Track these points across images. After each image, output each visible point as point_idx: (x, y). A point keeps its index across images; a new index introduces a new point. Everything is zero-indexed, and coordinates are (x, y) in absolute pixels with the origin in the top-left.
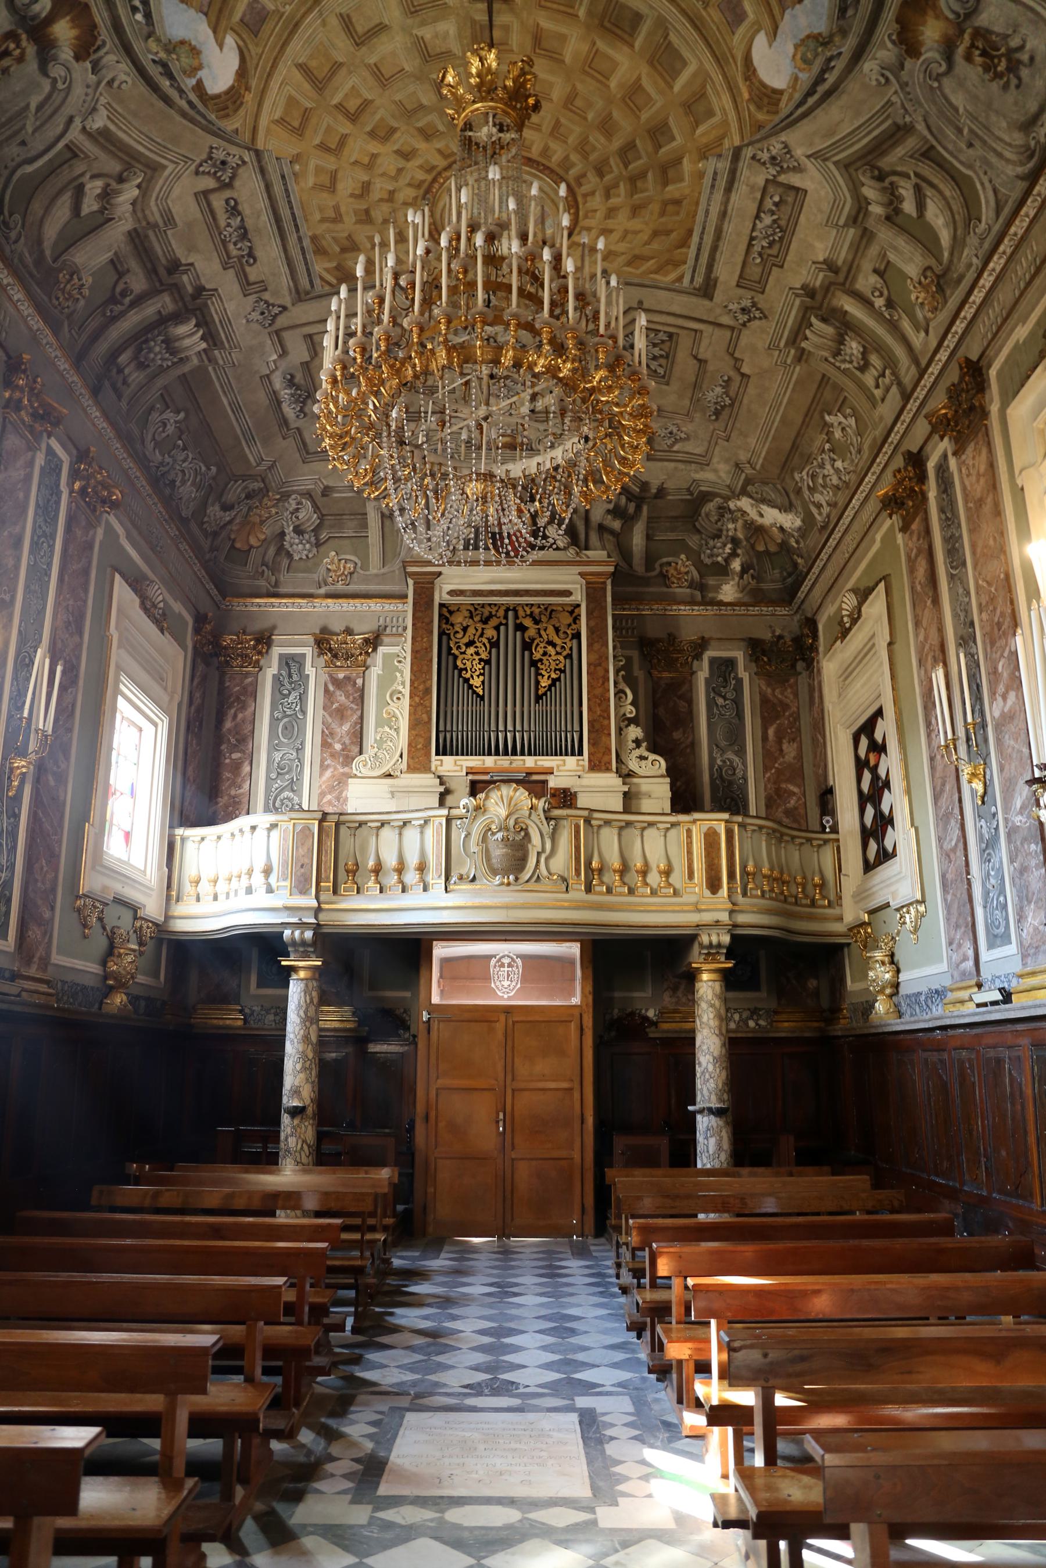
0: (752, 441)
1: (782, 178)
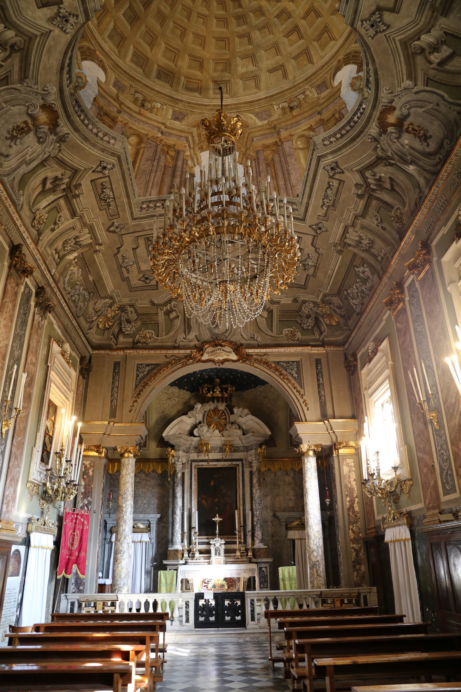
1: (55, 8)
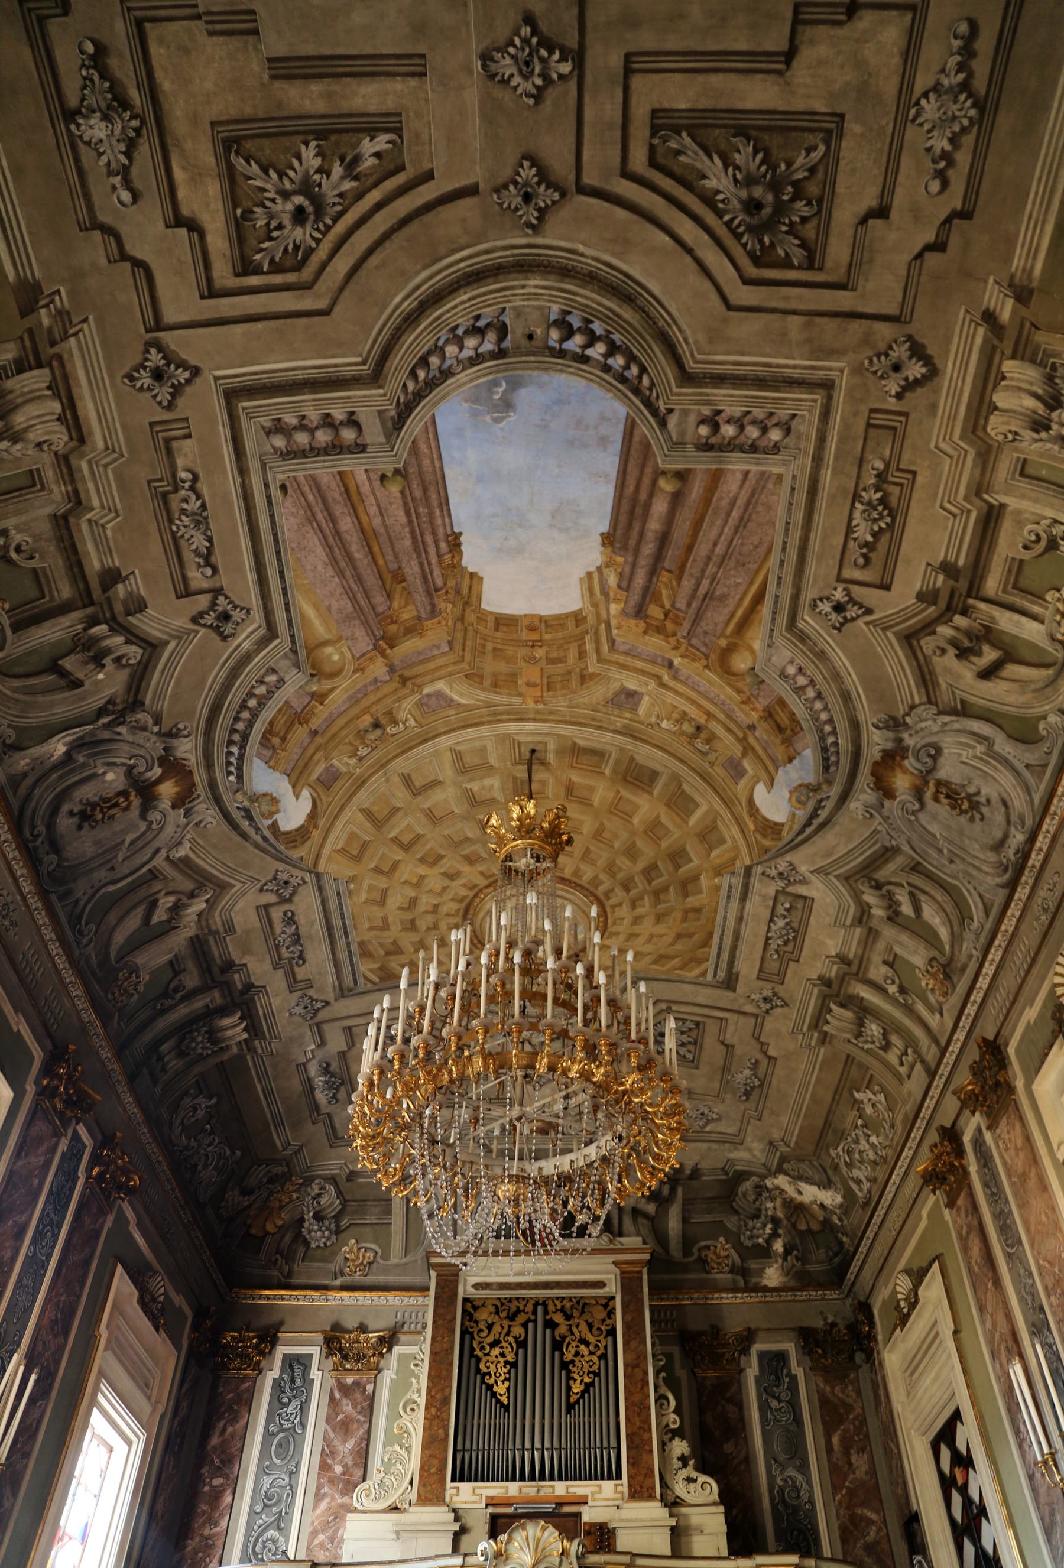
0: (784, 1120)
1: (790, 889)
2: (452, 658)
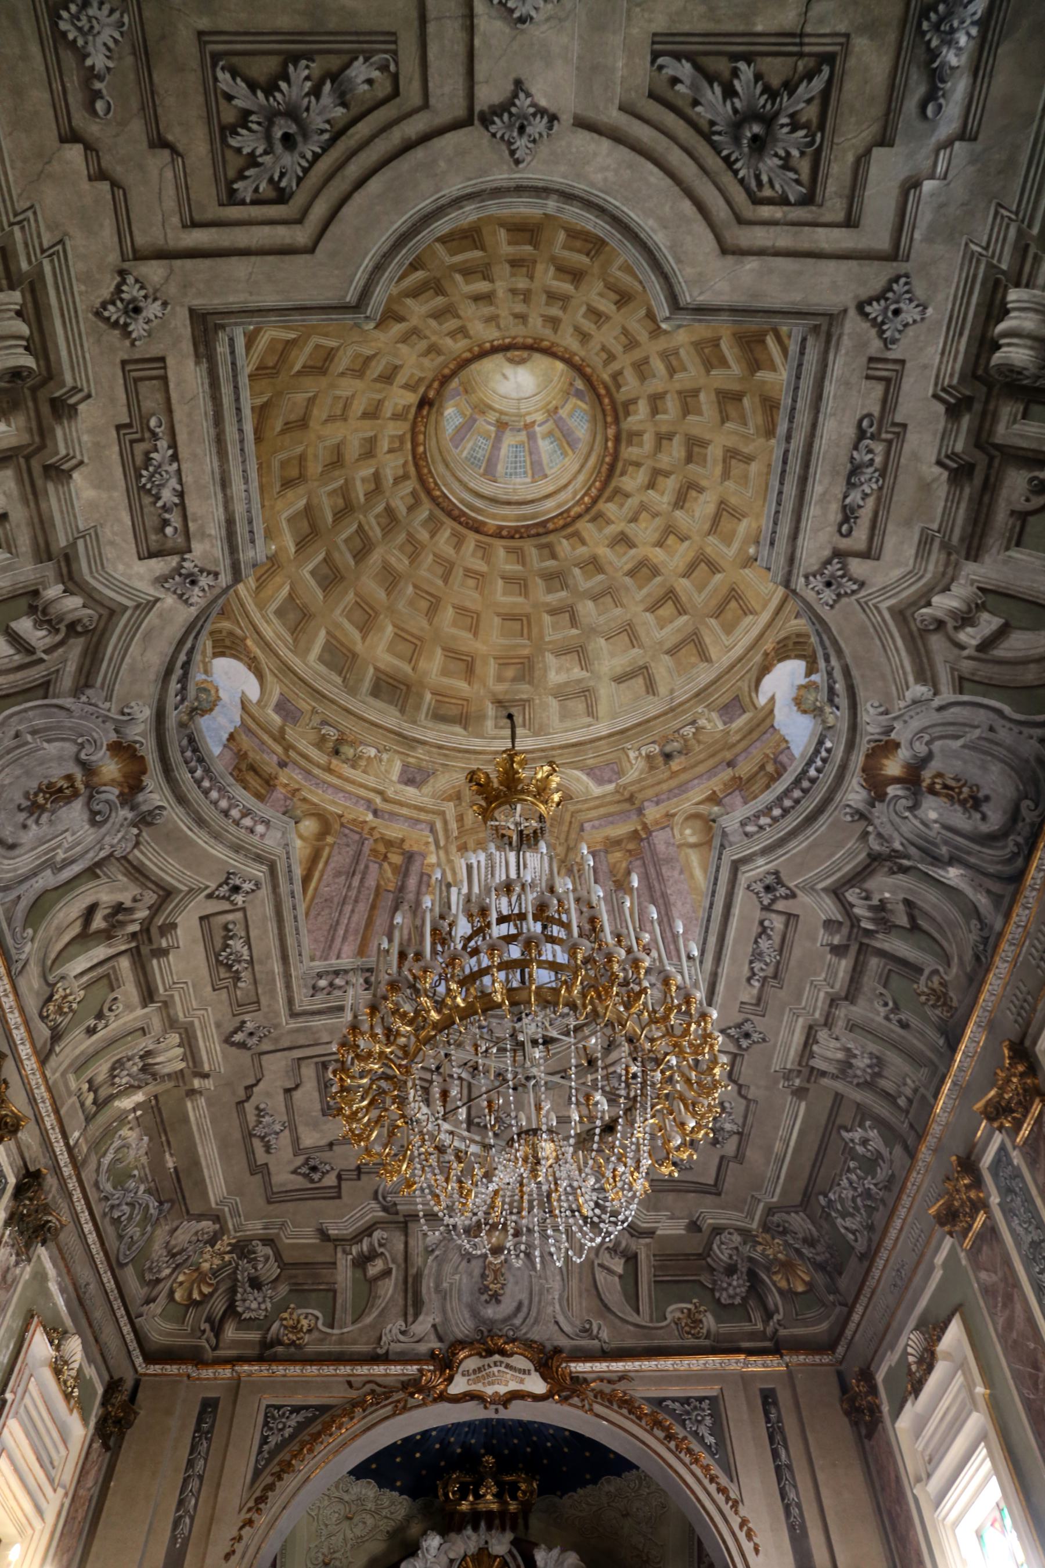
1: (174, 561)
2: (582, 817)
